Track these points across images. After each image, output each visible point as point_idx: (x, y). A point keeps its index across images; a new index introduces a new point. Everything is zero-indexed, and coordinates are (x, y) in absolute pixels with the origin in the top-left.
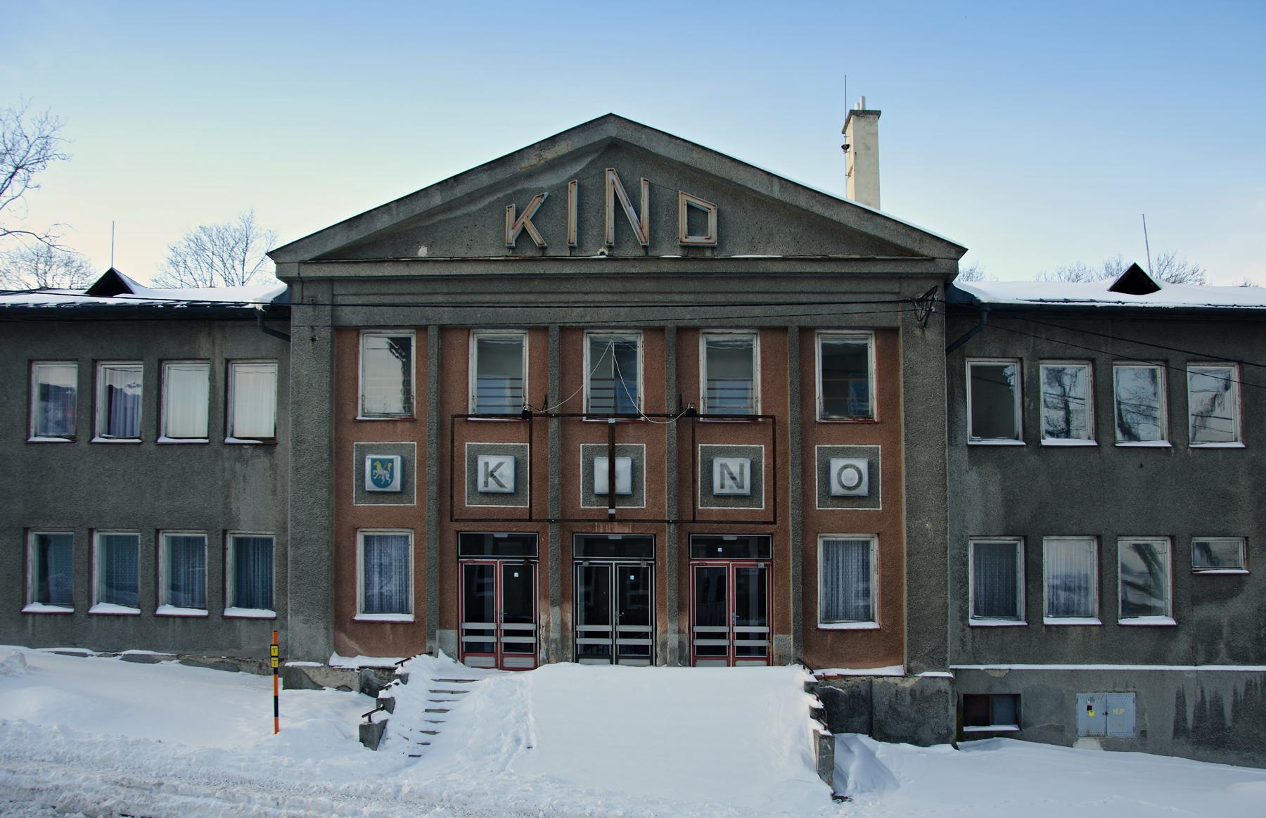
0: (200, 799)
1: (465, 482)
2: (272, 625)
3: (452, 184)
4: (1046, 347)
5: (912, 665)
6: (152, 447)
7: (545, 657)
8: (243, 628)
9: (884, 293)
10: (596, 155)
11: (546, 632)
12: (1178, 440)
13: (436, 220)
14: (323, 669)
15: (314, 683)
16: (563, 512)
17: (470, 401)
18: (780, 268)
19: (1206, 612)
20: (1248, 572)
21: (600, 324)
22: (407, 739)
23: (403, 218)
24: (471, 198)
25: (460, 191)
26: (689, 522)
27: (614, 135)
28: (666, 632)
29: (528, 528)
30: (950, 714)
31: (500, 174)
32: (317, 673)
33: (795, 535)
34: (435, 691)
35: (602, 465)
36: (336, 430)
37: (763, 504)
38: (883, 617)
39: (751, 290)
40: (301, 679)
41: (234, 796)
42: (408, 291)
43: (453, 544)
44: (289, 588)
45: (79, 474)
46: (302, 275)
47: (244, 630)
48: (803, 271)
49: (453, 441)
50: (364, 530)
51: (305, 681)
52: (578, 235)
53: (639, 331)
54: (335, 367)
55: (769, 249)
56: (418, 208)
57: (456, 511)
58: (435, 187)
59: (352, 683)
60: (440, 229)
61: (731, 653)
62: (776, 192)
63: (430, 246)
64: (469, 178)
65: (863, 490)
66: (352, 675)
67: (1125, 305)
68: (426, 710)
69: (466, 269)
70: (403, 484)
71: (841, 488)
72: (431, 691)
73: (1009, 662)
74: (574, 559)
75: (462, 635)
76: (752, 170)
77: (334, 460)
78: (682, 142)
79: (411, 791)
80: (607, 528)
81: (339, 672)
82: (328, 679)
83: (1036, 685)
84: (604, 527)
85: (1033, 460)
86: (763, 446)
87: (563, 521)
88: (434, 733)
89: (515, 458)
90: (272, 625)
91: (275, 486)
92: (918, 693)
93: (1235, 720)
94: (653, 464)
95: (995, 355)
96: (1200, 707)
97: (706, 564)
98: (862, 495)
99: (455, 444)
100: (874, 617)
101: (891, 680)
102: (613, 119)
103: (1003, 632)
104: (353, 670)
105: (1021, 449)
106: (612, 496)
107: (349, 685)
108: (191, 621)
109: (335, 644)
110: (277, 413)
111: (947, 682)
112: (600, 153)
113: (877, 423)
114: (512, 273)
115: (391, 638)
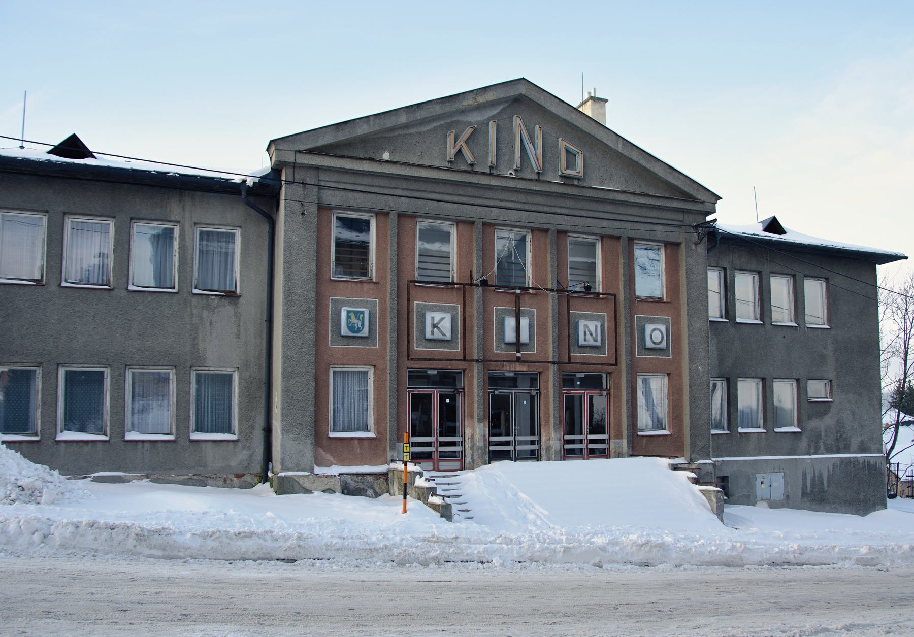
1: (414, 331)
2: (235, 446)
3: (415, 109)
5: (692, 456)
6: (124, 293)
8: (209, 450)
9: (674, 220)
10: (507, 105)
11: (471, 442)
12: (800, 322)
13: (396, 133)
14: (311, 477)
15: (304, 488)
18: (622, 197)
19: (815, 424)
20: (832, 400)
21: (509, 223)
23: (378, 129)
24: (423, 122)
25: (420, 115)
26: (566, 363)
27: (523, 93)
29: (461, 365)
31: (448, 108)
32: (306, 480)
33: (627, 373)
35: (510, 322)
37: (606, 352)
39: (602, 210)
40: (293, 485)
42: (377, 184)
45: (48, 314)
46: (297, 161)
47: (209, 452)
48: (634, 201)
51: (297, 488)
52: (497, 159)
53: (528, 230)
55: (611, 184)
56: (389, 123)
58: (403, 109)
59: (336, 487)
60: (399, 141)
61: (586, 452)
62: (620, 148)
63: (392, 153)
64: (427, 107)
67: (786, 240)
69: (424, 173)
70: (370, 330)
73: (722, 457)
76: (608, 131)
78: (566, 105)
81: (324, 478)
84: (510, 366)
85: (732, 331)
86: (606, 314)
87: (484, 361)
90: (235, 446)
91: (239, 331)
93: (828, 486)
94: (540, 323)
95: (713, 265)
96: (813, 479)
97: (571, 393)
102: (524, 82)
104: (335, 476)
105: (726, 323)
106: (518, 345)
108: (160, 444)
111: (712, 466)
112: (508, 104)
114: (456, 180)
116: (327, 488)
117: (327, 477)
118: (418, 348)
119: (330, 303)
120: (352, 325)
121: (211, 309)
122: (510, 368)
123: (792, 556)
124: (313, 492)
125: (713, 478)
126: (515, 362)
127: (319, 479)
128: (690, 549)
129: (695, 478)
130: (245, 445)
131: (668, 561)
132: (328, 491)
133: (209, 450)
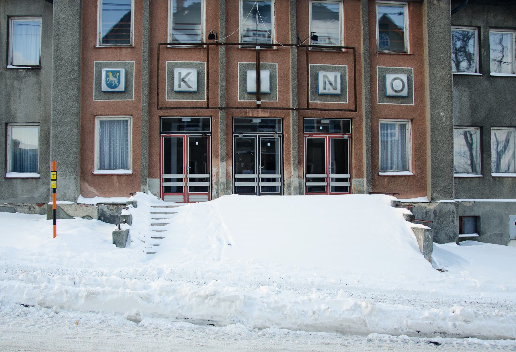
0: (5, 281)
4: (493, 21)
5: (434, 196)
7: (216, 194)
8: (19, 185)
11: (216, 178)
14: (73, 206)
16: (227, 103)
17: (169, 37)
22: (144, 242)
28: (290, 177)
29: (206, 113)
30: (455, 224)
32: (69, 208)
33: (367, 118)
34: (154, 213)
35: (252, 75)
36: (83, 54)
37: (347, 100)
38: (415, 167)
41: (35, 278)
43: (157, 124)
44: (51, 153)
49: (158, 59)
50: (99, 117)
54: (82, 14)
57: (160, 104)
61: (328, 189)
65: (405, 93)
66: (93, 209)
68: (152, 224)
71: (392, 91)
72: (151, 213)
73: (473, 198)
74: (233, 133)
75: (163, 182)
77: (81, 72)
79: (172, 272)
80: (254, 113)
81: (84, 207)
82: (77, 212)
83: (489, 210)
84: (253, 113)
85: (486, 84)
86: (347, 66)
87: (227, 108)
88: (161, 238)
89: (198, 71)
91: (40, 95)
92: (438, 212)
94: (282, 75)
95: (466, 24)
97: (314, 136)
98: (404, 96)
99: (160, 62)
100: (409, 168)
101: (423, 205)
103: (470, 181)
104: (93, 205)
105: (480, 77)
106: (258, 94)
107: (90, 215)
109: (80, 190)
110: (42, 49)
111: (454, 206)
113: (410, 55)
115: (117, 185)
116: (86, 215)
117: (86, 205)
118: (169, 99)
119: (94, 66)
120: (110, 82)
121: (20, 79)
122: (253, 115)
123: (450, 324)
124: (74, 218)
125: (455, 216)
126: (255, 108)
127: (80, 208)
128: (284, 306)
129: (410, 216)
130: (44, 181)
131: (245, 320)
132: (87, 217)
133: (19, 185)
